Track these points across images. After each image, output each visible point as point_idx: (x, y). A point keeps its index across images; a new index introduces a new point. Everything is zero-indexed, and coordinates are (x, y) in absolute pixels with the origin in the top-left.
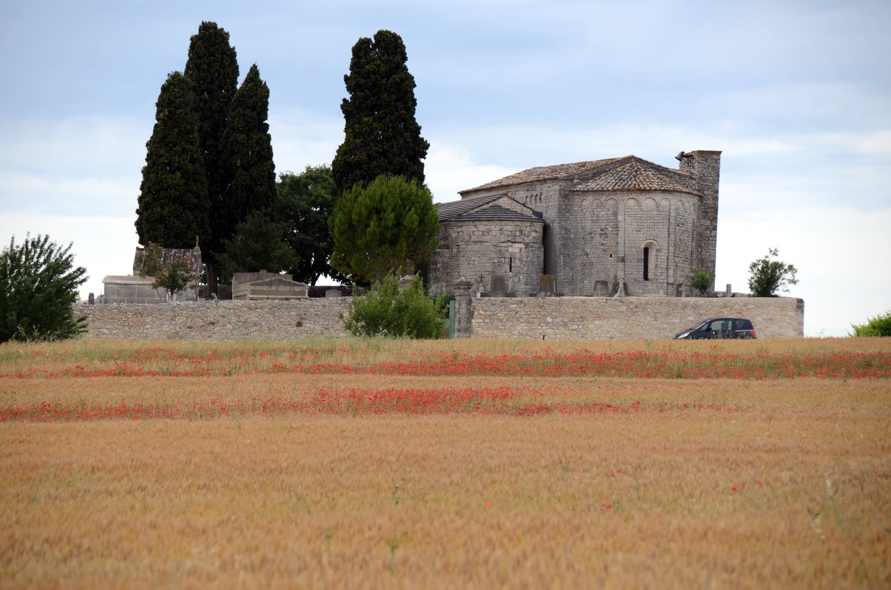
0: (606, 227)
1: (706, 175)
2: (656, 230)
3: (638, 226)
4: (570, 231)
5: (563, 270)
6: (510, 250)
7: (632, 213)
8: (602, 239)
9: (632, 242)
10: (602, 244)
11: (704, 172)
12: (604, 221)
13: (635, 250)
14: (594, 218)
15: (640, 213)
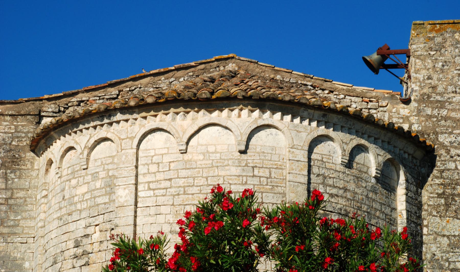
1: (440, 89)
7: (160, 176)
11: (434, 82)
12: (84, 215)
15: (183, 173)
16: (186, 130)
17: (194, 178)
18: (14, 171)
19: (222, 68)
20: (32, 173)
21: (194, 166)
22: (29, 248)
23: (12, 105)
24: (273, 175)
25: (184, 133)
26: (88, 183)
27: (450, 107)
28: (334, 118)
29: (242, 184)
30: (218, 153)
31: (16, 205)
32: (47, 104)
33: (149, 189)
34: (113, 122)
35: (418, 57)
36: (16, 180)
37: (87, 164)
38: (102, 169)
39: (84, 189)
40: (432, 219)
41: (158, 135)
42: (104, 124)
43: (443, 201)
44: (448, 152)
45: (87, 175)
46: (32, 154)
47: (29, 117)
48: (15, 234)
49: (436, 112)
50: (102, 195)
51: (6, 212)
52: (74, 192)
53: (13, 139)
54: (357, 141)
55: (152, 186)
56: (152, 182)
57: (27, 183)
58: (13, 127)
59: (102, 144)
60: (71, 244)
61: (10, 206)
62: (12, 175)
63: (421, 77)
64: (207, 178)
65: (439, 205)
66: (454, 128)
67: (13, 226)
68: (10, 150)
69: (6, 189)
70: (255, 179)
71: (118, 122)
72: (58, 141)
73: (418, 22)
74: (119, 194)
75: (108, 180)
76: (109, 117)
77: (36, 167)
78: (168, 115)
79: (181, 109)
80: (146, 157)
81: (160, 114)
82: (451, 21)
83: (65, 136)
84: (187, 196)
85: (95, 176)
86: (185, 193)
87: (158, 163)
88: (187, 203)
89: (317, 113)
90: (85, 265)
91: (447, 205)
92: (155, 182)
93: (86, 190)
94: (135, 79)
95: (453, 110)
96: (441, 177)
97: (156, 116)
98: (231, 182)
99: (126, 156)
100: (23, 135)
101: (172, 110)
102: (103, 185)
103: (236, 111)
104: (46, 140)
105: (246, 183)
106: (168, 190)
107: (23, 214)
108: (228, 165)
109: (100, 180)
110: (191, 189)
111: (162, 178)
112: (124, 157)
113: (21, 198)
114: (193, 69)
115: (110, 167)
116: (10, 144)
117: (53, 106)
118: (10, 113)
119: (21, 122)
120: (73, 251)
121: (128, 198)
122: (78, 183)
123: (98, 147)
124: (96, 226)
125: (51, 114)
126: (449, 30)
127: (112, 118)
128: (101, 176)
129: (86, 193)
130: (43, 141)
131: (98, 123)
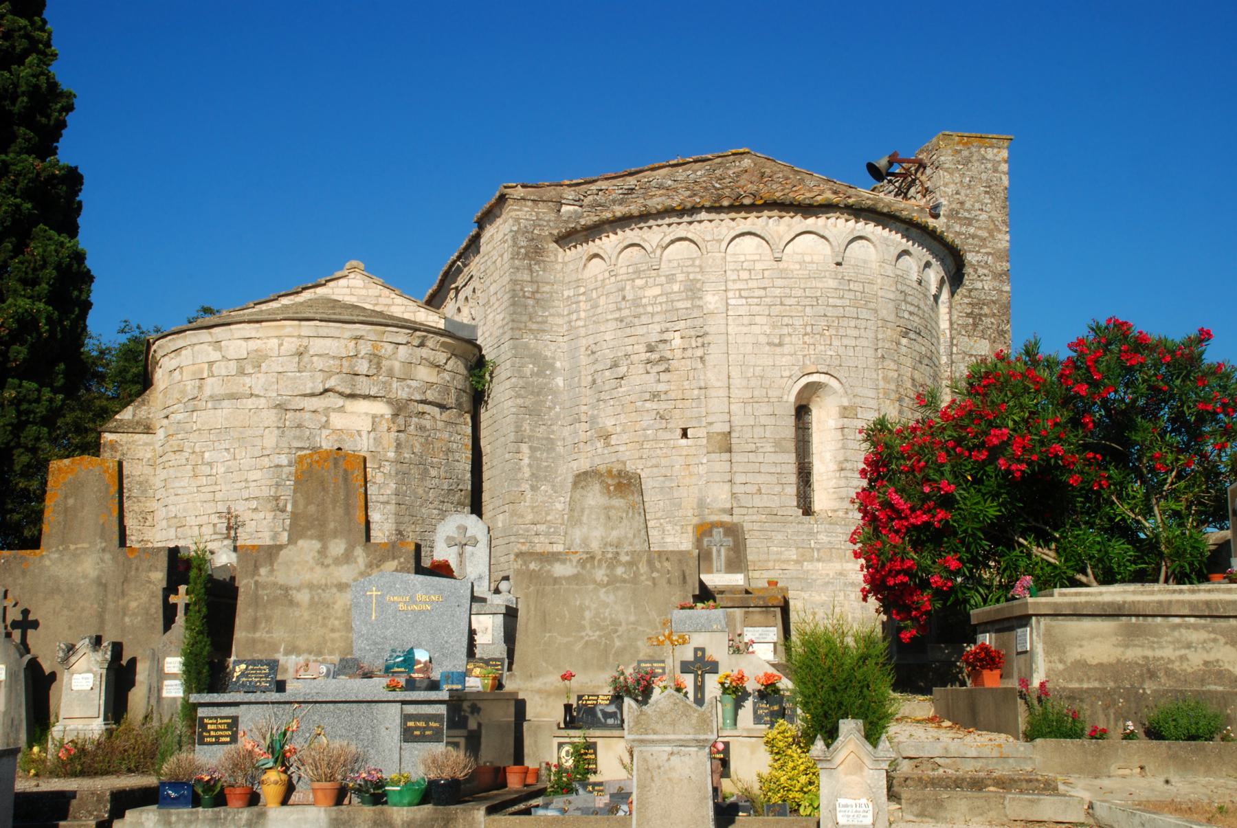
0: (665, 336)
1: (968, 205)
2: (836, 342)
3: (774, 326)
4: (552, 367)
5: (529, 495)
6: (337, 421)
7: (752, 284)
8: (651, 378)
9: (753, 383)
10: (655, 396)
11: (962, 198)
12: (657, 318)
13: (766, 409)
14: (626, 313)
15: (779, 282)
17: (791, 288)
18: (538, 263)
19: (737, 164)
20: (556, 266)
22: (559, 347)
24: (866, 290)
25: (780, 239)
26: (662, 285)
27: (977, 225)
28: (914, 231)
29: (839, 298)
32: (567, 189)
33: (741, 297)
35: (946, 170)
36: (541, 273)
39: (657, 291)
40: (962, 339)
41: (748, 238)
43: (971, 321)
44: (976, 271)
45: (659, 276)
46: (555, 245)
47: (550, 204)
48: (544, 331)
49: (964, 229)
51: (534, 307)
52: (640, 293)
53: (535, 226)
54: (930, 258)
55: (743, 293)
59: (678, 244)
61: (538, 301)
62: (537, 267)
63: (949, 191)
64: (804, 289)
65: (967, 325)
66: (980, 247)
68: (532, 240)
69: (532, 282)
71: (700, 222)
73: (947, 133)
76: (691, 215)
82: (979, 135)
83: (616, 234)
85: (671, 278)
86: (782, 304)
87: (750, 270)
89: (904, 226)
91: (975, 325)
94: (653, 169)
95: (980, 228)
96: (970, 297)
101: (766, 213)
102: (682, 289)
103: (832, 220)
105: (843, 297)
108: (825, 277)
109: (678, 284)
111: (755, 286)
114: (709, 162)
115: (690, 269)
119: (542, 208)
120: (645, 356)
121: (718, 305)
125: (572, 202)
126: (975, 144)
127: (694, 216)
131: (679, 220)
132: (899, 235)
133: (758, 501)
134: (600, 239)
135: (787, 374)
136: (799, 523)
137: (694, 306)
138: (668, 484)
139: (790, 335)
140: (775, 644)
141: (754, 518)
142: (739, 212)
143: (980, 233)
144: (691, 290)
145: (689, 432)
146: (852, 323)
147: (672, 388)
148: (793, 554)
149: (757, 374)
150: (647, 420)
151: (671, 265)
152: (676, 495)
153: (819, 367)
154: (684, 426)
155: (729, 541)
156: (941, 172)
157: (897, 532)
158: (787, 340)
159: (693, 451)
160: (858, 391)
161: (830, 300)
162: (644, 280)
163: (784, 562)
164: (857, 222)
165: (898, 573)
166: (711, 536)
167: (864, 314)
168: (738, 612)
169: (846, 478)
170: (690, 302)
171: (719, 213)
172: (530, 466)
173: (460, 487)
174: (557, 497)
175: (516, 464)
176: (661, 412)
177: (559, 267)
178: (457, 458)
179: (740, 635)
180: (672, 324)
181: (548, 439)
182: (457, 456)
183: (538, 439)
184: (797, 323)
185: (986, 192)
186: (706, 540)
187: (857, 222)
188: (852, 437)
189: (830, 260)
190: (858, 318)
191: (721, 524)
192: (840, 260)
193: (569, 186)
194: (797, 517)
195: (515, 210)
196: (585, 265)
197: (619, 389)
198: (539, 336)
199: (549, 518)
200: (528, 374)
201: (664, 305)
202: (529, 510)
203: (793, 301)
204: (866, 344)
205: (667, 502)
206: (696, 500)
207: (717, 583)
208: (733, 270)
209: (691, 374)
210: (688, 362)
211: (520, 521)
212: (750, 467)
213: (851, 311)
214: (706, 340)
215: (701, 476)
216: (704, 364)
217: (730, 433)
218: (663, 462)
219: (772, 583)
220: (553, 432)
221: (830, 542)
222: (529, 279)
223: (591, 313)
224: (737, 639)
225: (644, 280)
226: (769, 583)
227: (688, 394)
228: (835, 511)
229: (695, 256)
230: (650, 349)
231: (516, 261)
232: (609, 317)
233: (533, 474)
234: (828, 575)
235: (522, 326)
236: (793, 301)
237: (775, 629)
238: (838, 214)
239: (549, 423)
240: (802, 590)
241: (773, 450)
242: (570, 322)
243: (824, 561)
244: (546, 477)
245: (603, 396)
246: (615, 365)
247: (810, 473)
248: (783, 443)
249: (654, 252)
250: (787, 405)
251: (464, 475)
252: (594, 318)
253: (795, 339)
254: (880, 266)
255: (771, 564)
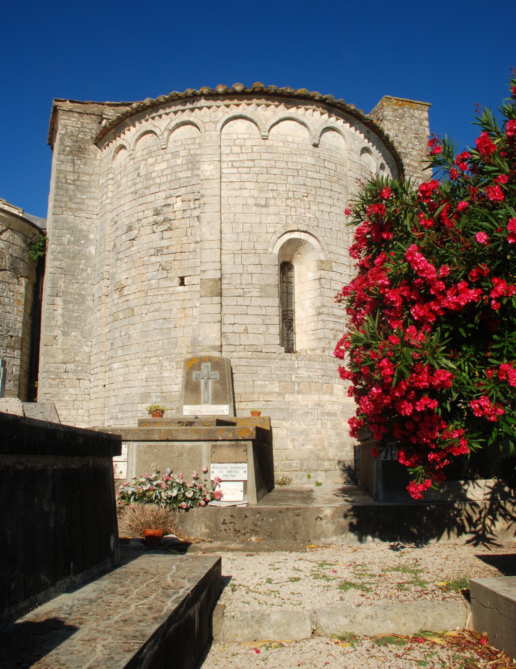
0: (169, 201)
1: (404, 144)
2: (314, 207)
3: (261, 191)
4: (86, 238)
5: (60, 339)
7: (243, 157)
8: (157, 236)
9: (242, 237)
10: (159, 251)
12: (163, 187)
13: (253, 259)
15: (265, 156)
16: (268, 119)
17: (276, 161)
18: (80, 159)
20: (95, 162)
21: (276, 151)
22: (93, 223)
23: (79, 105)
24: (338, 170)
25: (267, 121)
26: (168, 161)
28: (373, 134)
30: (295, 143)
31: (82, 186)
33: (233, 167)
34: (195, 108)
35: (389, 121)
37: (167, 144)
38: (183, 149)
39: (164, 165)
41: (240, 122)
42: (186, 110)
45: (166, 154)
46: (95, 147)
47: (93, 116)
48: (81, 210)
50: (184, 171)
51: (74, 191)
52: (151, 169)
53: (79, 132)
56: (236, 161)
57: (91, 170)
58: (79, 123)
59: (182, 128)
60: (150, 213)
64: (287, 162)
66: (413, 172)
67: (79, 203)
68: (77, 141)
69: (73, 172)
70: (325, 169)
71: (200, 108)
72: (132, 128)
73: (388, 96)
74: (204, 168)
75: (190, 157)
77: (98, 158)
78: (250, 106)
79: (263, 101)
80: (229, 139)
81: (244, 103)
82: (409, 100)
84: (270, 176)
85: (175, 155)
86: (267, 173)
87: (241, 146)
88: (270, 181)
89: (366, 128)
90: (166, 230)
92: (238, 161)
93: (166, 167)
95: (412, 160)
97: (238, 105)
98: (307, 168)
99: (211, 137)
100: (88, 131)
101: (255, 101)
102: (184, 162)
104: (116, 130)
106: (252, 169)
107: (88, 194)
108: (304, 154)
109: (181, 158)
110: (273, 170)
112: (208, 137)
113: (86, 181)
115: (191, 147)
116: (77, 136)
117: (112, 111)
118: (78, 110)
119: (86, 120)
120: (152, 219)
122: (156, 161)
123: (177, 130)
124: (177, 197)
126: (407, 106)
127: (195, 103)
128: (182, 155)
129: (165, 169)
130: (113, 131)
131: (182, 108)
132: (362, 136)
133: (245, 340)
134: (124, 133)
135: (272, 230)
136: (282, 359)
137: (193, 176)
138: (166, 326)
139: (275, 198)
140: (245, 482)
141: (241, 354)
142: (232, 99)
143: (413, 163)
144: (192, 163)
145: (186, 280)
146: (328, 194)
147: (173, 243)
148: (275, 387)
149: (245, 230)
150: (152, 272)
151: (176, 144)
152: (173, 334)
153: (299, 226)
154: (181, 275)
155: (216, 374)
156: (385, 122)
157: (419, 324)
158: (272, 202)
159: (188, 296)
160: (333, 248)
161: (309, 173)
162: (154, 158)
163: (267, 394)
164: (330, 117)
165: (419, 393)
166: (200, 369)
167: (336, 188)
168: (205, 446)
169: (323, 320)
170: (190, 172)
171: (216, 100)
172: (63, 315)
173: (10, 334)
174: (85, 342)
175: (51, 313)
176: (163, 264)
177: (97, 163)
178: (8, 310)
179: (206, 472)
180: (175, 191)
181: (79, 294)
182: (8, 308)
183: (71, 294)
184: (281, 189)
185: (416, 138)
186: (195, 374)
187: (330, 117)
188: (328, 287)
189: (309, 143)
190: (332, 190)
191: (209, 359)
192: (317, 142)
193: (108, 105)
194: (280, 353)
195: (64, 119)
196: (114, 157)
197: (133, 249)
198: (76, 214)
199: (77, 358)
200: (66, 242)
201: (169, 176)
202: (60, 351)
203: (277, 171)
204: (339, 212)
205: (165, 341)
206: (190, 339)
207: (204, 413)
208: (227, 146)
209: (189, 231)
210: (187, 221)
211: (52, 360)
212: (238, 310)
213: (326, 184)
214: (201, 201)
215: (194, 318)
216: (200, 222)
217: (221, 279)
218: (164, 306)
219: (256, 413)
220: (84, 289)
221: (309, 377)
222: (72, 170)
223: (116, 193)
224: (203, 477)
225: (154, 158)
226: (253, 413)
227: (185, 248)
228: (313, 350)
229: (195, 136)
230: (157, 213)
231: (62, 156)
232: (127, 192)
233: (65, 322)
234: (307, 405)
235: (63, 205)
236: (277, 171)
237: (245, 465)
238: (314, 107)
239: (82, 281)
240: (284, 419)
241: (258, 294)
242: (101, 203)
243: (303, 394)
244: (76, 325)
245: (121, 256)
246: (130, 228)
247: (292, 320)
248: (268, 288)
249: (162, 134)
250: (272, 256)
251: (15, 325)
252: (118, 196)
253: (278, 202)
254: (349, 153)
255: (255, 397)
